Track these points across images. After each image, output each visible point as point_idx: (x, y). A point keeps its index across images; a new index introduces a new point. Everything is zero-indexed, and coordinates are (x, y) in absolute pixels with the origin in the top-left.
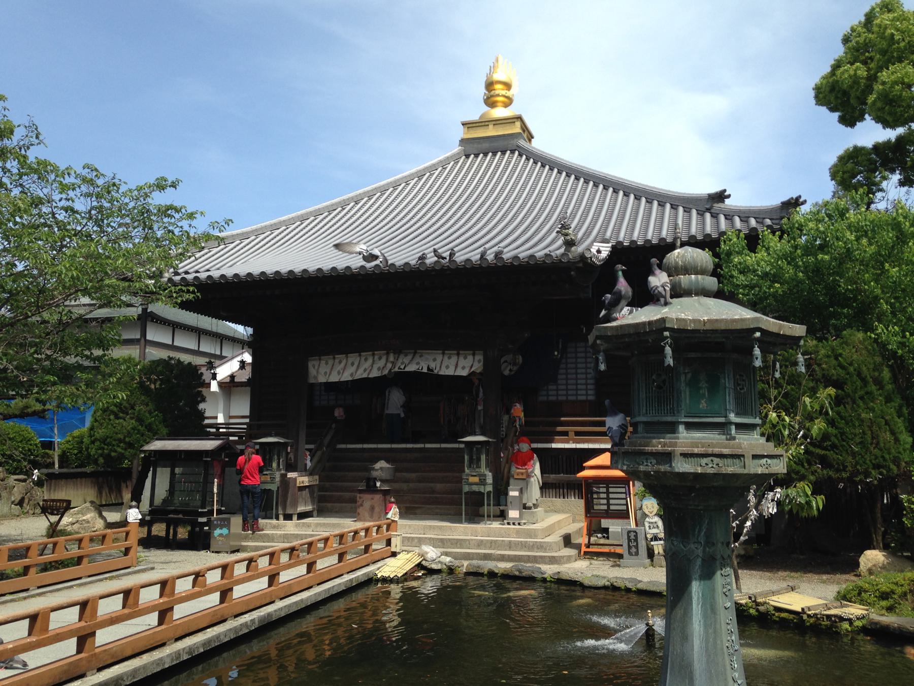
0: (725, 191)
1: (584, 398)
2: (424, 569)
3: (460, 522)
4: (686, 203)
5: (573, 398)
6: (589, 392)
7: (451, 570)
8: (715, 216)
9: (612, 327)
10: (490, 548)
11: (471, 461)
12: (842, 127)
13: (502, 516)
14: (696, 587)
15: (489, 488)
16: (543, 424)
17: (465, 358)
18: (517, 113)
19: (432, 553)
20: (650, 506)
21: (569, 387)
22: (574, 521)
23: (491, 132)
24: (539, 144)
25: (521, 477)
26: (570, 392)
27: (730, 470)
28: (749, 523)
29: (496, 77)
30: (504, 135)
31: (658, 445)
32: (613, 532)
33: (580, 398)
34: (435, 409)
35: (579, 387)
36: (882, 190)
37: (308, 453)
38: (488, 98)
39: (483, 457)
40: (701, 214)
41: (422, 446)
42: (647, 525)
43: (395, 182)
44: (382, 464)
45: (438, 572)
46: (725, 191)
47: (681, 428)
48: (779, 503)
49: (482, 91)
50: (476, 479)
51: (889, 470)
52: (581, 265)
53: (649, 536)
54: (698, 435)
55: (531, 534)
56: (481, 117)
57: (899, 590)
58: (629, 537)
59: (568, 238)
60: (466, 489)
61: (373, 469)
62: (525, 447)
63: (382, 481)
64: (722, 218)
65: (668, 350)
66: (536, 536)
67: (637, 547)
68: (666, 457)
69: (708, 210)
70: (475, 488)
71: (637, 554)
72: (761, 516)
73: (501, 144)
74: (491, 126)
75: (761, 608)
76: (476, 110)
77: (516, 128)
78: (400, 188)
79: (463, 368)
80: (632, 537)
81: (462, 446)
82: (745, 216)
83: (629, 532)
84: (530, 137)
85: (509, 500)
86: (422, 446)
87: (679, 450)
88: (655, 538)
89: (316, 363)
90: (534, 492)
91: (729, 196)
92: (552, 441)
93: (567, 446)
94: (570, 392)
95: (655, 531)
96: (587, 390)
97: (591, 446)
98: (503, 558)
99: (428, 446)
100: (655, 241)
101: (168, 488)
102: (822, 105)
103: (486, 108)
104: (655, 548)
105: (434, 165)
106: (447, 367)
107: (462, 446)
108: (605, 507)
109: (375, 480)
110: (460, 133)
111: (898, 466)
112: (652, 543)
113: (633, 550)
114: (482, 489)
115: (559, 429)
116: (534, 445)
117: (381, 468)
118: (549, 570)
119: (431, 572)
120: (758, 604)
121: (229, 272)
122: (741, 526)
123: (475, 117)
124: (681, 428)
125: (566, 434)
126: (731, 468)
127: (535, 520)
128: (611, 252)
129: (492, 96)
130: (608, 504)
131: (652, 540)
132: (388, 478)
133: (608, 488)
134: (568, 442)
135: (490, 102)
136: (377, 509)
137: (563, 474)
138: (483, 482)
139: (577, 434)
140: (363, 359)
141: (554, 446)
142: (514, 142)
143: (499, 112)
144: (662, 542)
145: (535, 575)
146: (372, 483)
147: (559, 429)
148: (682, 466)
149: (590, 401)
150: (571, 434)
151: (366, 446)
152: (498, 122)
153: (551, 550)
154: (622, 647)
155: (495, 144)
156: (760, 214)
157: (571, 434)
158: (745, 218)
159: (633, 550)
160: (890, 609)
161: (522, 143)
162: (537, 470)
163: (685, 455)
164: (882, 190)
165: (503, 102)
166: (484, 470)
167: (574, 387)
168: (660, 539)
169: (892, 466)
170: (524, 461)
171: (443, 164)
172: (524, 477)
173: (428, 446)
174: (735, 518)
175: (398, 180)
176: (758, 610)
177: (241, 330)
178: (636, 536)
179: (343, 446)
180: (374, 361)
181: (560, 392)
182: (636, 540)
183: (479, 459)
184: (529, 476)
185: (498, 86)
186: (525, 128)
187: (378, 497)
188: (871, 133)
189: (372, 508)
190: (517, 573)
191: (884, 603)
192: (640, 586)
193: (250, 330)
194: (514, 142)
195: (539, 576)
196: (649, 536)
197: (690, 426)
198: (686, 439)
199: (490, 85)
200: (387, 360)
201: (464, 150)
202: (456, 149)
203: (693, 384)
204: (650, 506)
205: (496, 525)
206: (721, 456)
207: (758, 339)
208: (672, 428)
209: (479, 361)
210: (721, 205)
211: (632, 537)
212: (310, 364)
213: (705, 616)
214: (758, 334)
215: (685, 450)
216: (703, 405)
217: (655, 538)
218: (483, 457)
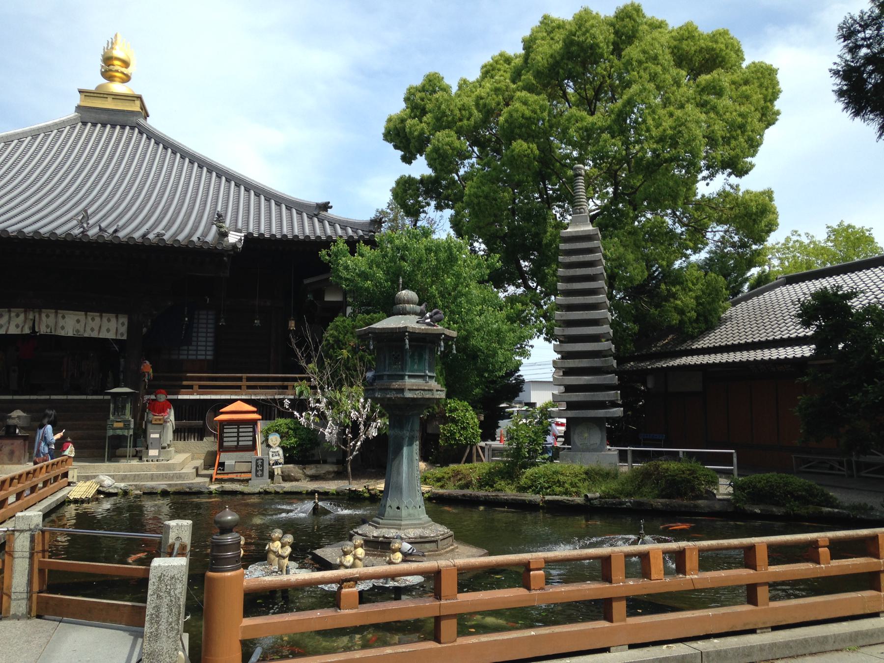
1: (203, 357)
2: (103, 494)
3: (103, 461)
4: (291, 205)
7: (125, 493)
8: (321, 221)
10: (133, 481)
11: (116, 409)
13: (138, 456)
14: (405, 449)
15: (131, 432)
16: (171, 377)
18: (137, 93)
19: (108, 481)
22: (192, 459)
23: (109, 104)
24: (154, 122)
25: (158, 422)
27: (427, 396)
28: (359, 443)
29: (116, 53)
30: (123, 111)
31: (396, 385)
32: (229, 465)
33: (200, 357)
34: (97, 362)
36: (424, 212)
38: (106, 71)
39: (128, 406)
40: (310, 218)
41: (48, 397)
42: (271, 454)
43: (7, 137)
44: (17, 413)
45: (116, 494)
47: (406, 377)
48: (379, 429)
49: (98, 64)
50: (121, 425)
51: (434, 409)
53: (271, 462)
54: (413, 381)
55: (169, 467)
56: (97, 88)
57: (446, 476)
58: (257, 463)
59: (222, 230)
60: (110, 433)
61: (10, 417)
62: (162, 398)
63: (22, 428)
65: (407, 341)
66: (174, 469)
67: (262, 471)
68: (402, 390)
69: (316, 215)
70: (119, 432)
71: (262, 475)
72: (367, 438)
73: (120, 118)
74: (110, 99)
75: (372, 492)
76: (94, 80)
77: (136, 107)
79: (108, 330)
80: (260, 463)
81: (109, 397)
82: (344, 225)
83: (257, 460)
84: (147, 115)
85: (149, 442)
86: (48, 397)
87: (407, 387)
88: (277, 463)
90: (170, 435)
91: (331, 207)
92: (178, 394)
93: (192, 397)
96: (206, 350)
99: (53, 397)
100: (279, 236)
102: (390, 141)
103: (104, 81)
106: (92, 330)
107: (107, 397)
108: (235, 444)
109: (15, 427)
110: (77, 100)
111: (439, 407)
113: (260, 473)
114: (126, 433)
115: (185, 383)
116: (170, 397)
117: (19, 417)
119: (109, 495)
120: (369, 490)
122: (355, 445)
123: (92, 88)
124: (406, 377)
125: (191, 387)
126: (428, 395)
127: (169, 457)
130: (238, 441)
132: (25, 425)
133: (238, 428)
134: (192, 394)
135: (108, 75)
136: (17, 453)
137: (195, 422)
138: (126, 427)
139: (201, 387)
141: (180, 397)
142: (134, 119)
143: (116, 87)
145: (203, 490)
146: (12, 430)
147: (185, 383)
148: (408, 395)
149: (208, 360)
150: (196, 388)
151: (32, 397)
152: (117, 97)
153: (189, 479)
154: (302, 515)
155: (115, 118)
156: (355, 226)
157: (196, 388)
158: (344, 228)
159: (260, 473)
160: (442, 487)
161: (141, 121)
162: (172, 418)
163: (409, 390)
164: (424, 212)
165: (120, 78)
166: (128, 416)
169: (436, 407)
170: (161, 409)
171: (59, 127)
172: (161, 422)
173: (53, 397)
174: (352, 440)
175: (11, 136)
176: (370, 494)
178: (263, 463)
180: (10, 318)
182: (262, 465)
183: (124, 408)
184: (166, 422)
185: (116, 62)
186: (143, 107)
187: (18, 442)
188: (420, 168)
189: (12, 453)
190: (188, 490)
191: (439, 484)
192: (285, 490)
194: (134, 119)
196: (271, 462)
197: (410, 376)
198: (409, 382)
199: (108, 60)
200: (26, 318)
202: (69, 112)
203: (412, 356)
205: (135, 462)
206: (424, 390)
208: (402, 377)
210: (324, 213)
211: (260, 463)
213: (408, 463)
215: (410, 387)
216: (416, 367)
217: (277, 463)
218: (128, 406)
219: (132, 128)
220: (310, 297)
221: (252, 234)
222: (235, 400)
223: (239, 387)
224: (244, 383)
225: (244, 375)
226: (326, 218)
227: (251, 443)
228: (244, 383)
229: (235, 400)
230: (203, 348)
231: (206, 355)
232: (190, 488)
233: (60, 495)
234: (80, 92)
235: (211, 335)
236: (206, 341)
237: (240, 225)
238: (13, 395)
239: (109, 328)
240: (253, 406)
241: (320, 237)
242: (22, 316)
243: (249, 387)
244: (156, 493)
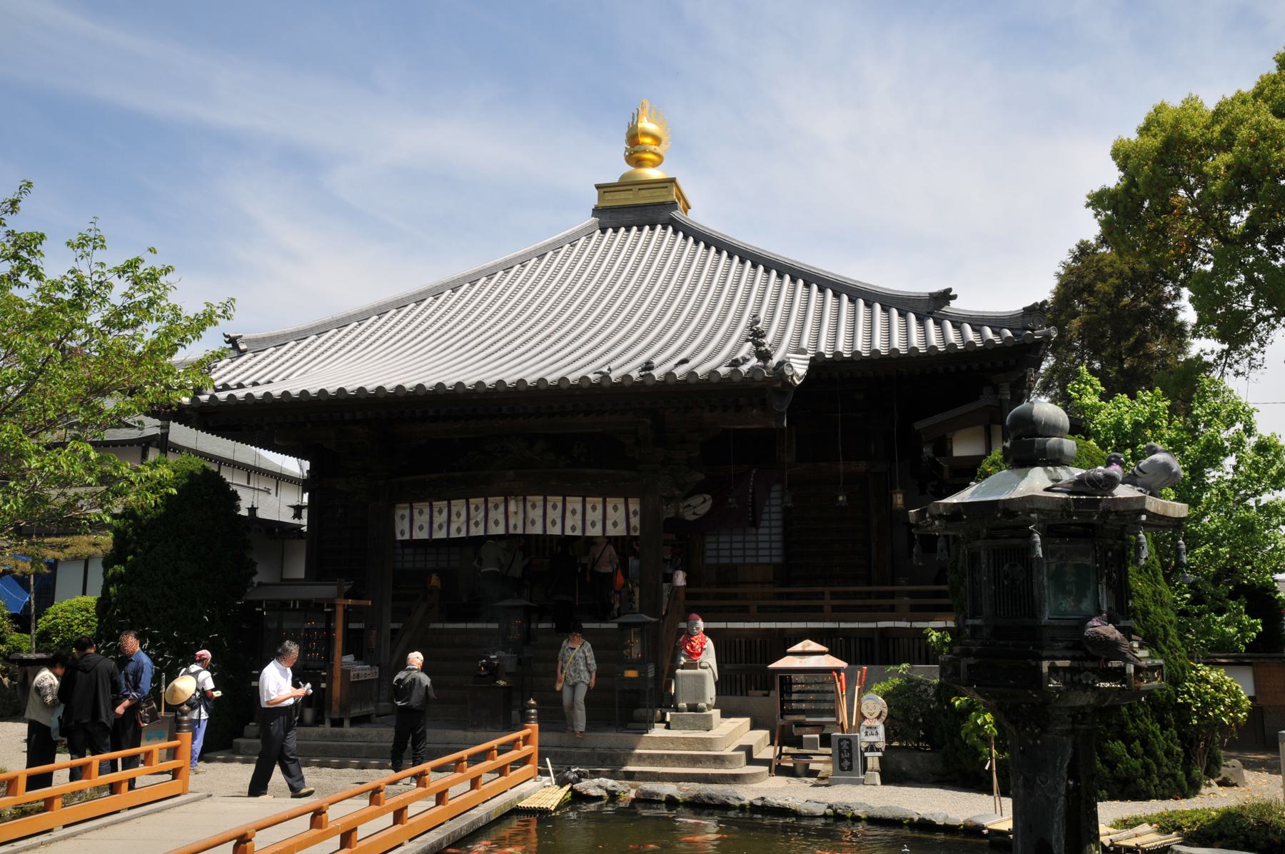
0: (950, 290)
1: (766, 560)
4: (889, 302)
5: (753, 560)
6: (774, 552)
8: (938, 323)
9: (946, 504)
21: (747, 545)
24: (699, 215)
26: (748, 553)
33: (762, 560)
34: (561, 584)
35: (761, 545)
38: (630, 154)
40: (921, 321)
43: (506, 262)
46: (950, 290)
52: (779, 385)
58: (840, 746)
64: (948, 324)
67: (850, 759)
71: (850, 768)
76: (615, 169)
78: (513, 271)
84: (687, 207)
88: (872, 748)
91: (955, 297)
94: (748, 553)
95: (872, 739)
98: (676, 778)
100: (865, 354)
103: (628, 168)
104: (869, 761)
105: (559, 241)
110: (593, 199)
112: (866, 754)
113: (845, 746)
118: (747, 794)
121: (295, 388)
123: (614, 179)
128: (810, 366)
129: (636, 152)
131: (866, 750)
135: (635, 159)
144: (880, 754)
145: (731, 802)
151: (470, 626)
158: (977, 328)
159: (845, 746)
167: (754, 545)
168: (878, 750)
177: (294, 466)
179: (439, 626)
181: (734, 553)
193: (307, 465)
195: (737, 803)
204: (871, 706)
207: (1144, 524)
214: (1144, 517)
217: (872, 748)
220: (927, 450)
221: (841, 354)
223: (820, 609)
224: (828, 603)
225: (827, 590)
226: (947, 316)
227: (534, 820)
230: (763, 544)
232: (711, 799)
233: (511, 795)
234: (598, 187)
235: (778, 523)
236: (770, 534)
237: (805, 343)
238: (488, 622)
241: (954, 345)
244: (659, 802)
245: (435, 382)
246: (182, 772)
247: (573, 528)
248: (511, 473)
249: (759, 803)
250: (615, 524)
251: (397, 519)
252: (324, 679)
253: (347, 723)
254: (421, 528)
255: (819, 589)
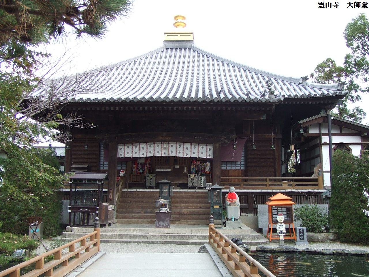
4: (291, 81)
6: (242, 166)
12: (322, 59)
17: (172, 146)
20: (281, 218)
24: (197, 44)
33: (237, 168)
37: (237, 195)
67: (303, 236)
71: (303, 239)
88: (281, 233)
89: (123, 147)
95: (281, 229)
97: (274, 191)
101: (89, 216)
113: (302, 237)
140: (148, 146)
143: (180, 29)
149: (242, 170)
150: (242, 185)
159: (302, 237)
168: (283, 233)
178: (303, 231)
201: (166, 46)
202: (161, 45)
204: (281, 218)
209: (210, 149)
212: (119, 147)
219: (185, 49)
222: (277, 193)
223: (265, 185)
224: (268, 183)
225: (268, 178)
228: (268, 183)
229: (277, 193)
231: (240, 167)
239: (203, 152)
240: (288, 196)
242: (138, 147)
243: (271, 185)
245: (86, 98)
246: (98, 244)
247: (165, 153)
248: (165, 133)
249: (307, 251)
250: (128, 153)
251: (119, 150)
252: (98, 210)
253: (107, 225)
254: (150, 152)
255: (265, 178)
